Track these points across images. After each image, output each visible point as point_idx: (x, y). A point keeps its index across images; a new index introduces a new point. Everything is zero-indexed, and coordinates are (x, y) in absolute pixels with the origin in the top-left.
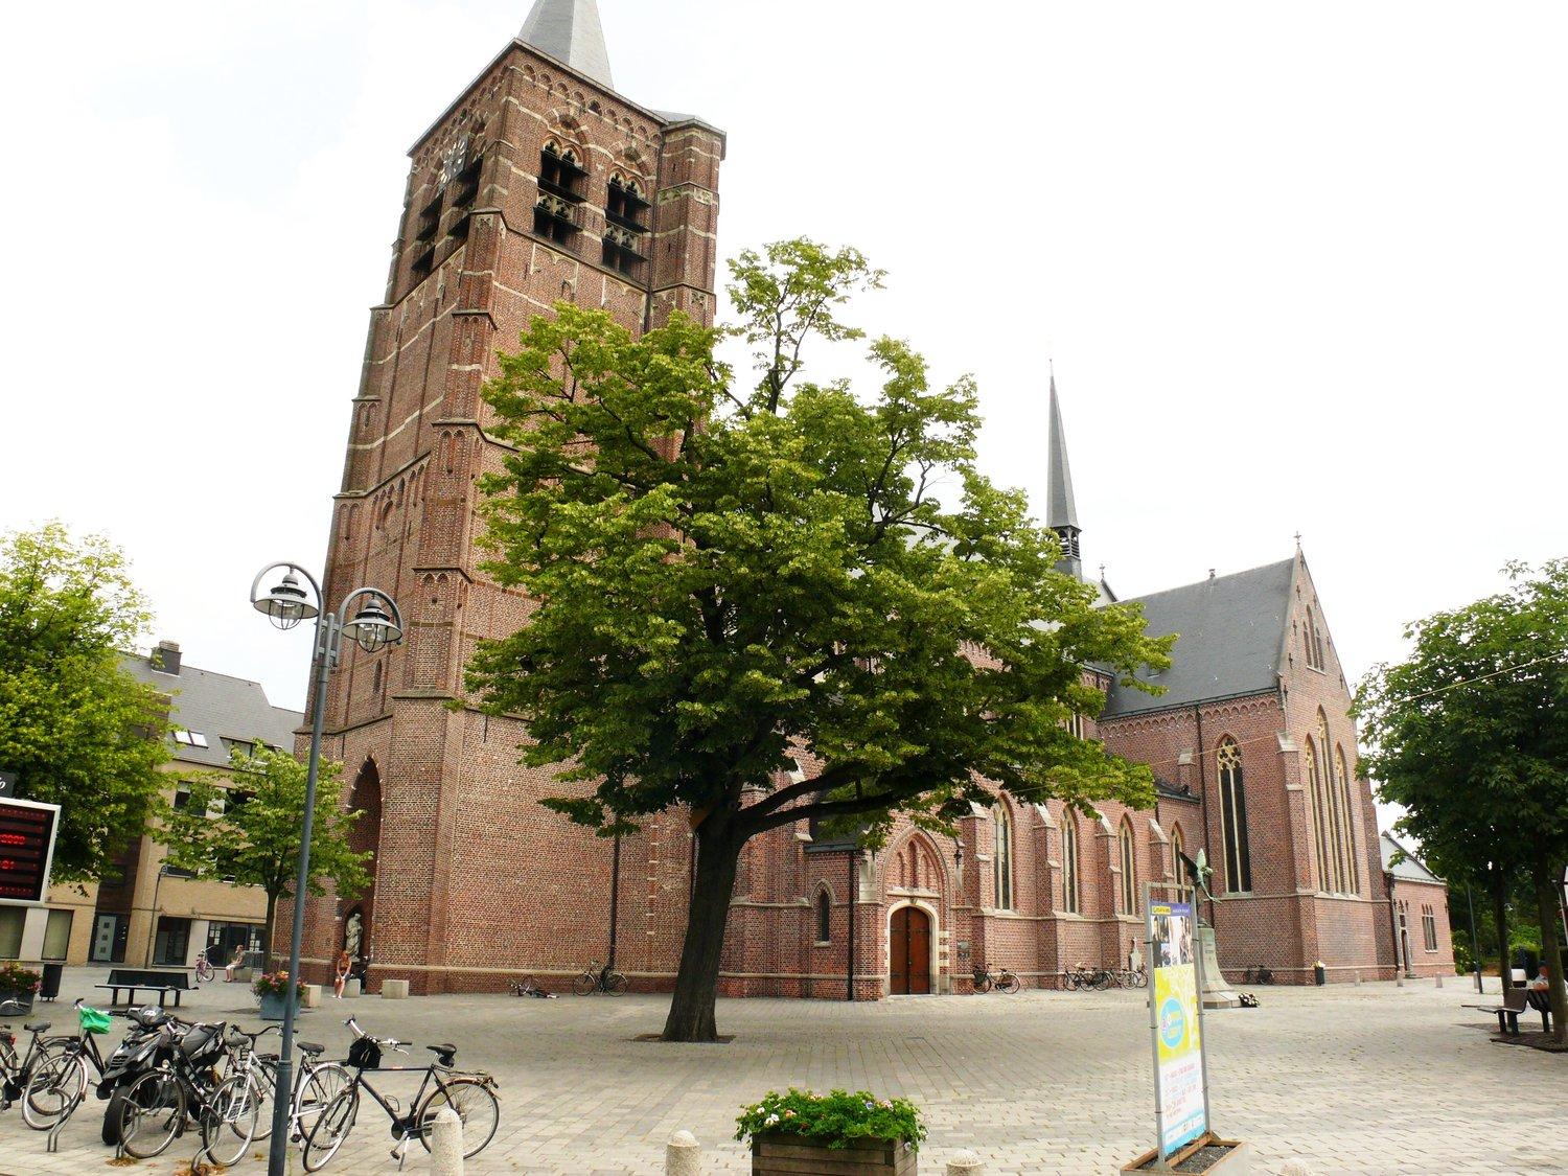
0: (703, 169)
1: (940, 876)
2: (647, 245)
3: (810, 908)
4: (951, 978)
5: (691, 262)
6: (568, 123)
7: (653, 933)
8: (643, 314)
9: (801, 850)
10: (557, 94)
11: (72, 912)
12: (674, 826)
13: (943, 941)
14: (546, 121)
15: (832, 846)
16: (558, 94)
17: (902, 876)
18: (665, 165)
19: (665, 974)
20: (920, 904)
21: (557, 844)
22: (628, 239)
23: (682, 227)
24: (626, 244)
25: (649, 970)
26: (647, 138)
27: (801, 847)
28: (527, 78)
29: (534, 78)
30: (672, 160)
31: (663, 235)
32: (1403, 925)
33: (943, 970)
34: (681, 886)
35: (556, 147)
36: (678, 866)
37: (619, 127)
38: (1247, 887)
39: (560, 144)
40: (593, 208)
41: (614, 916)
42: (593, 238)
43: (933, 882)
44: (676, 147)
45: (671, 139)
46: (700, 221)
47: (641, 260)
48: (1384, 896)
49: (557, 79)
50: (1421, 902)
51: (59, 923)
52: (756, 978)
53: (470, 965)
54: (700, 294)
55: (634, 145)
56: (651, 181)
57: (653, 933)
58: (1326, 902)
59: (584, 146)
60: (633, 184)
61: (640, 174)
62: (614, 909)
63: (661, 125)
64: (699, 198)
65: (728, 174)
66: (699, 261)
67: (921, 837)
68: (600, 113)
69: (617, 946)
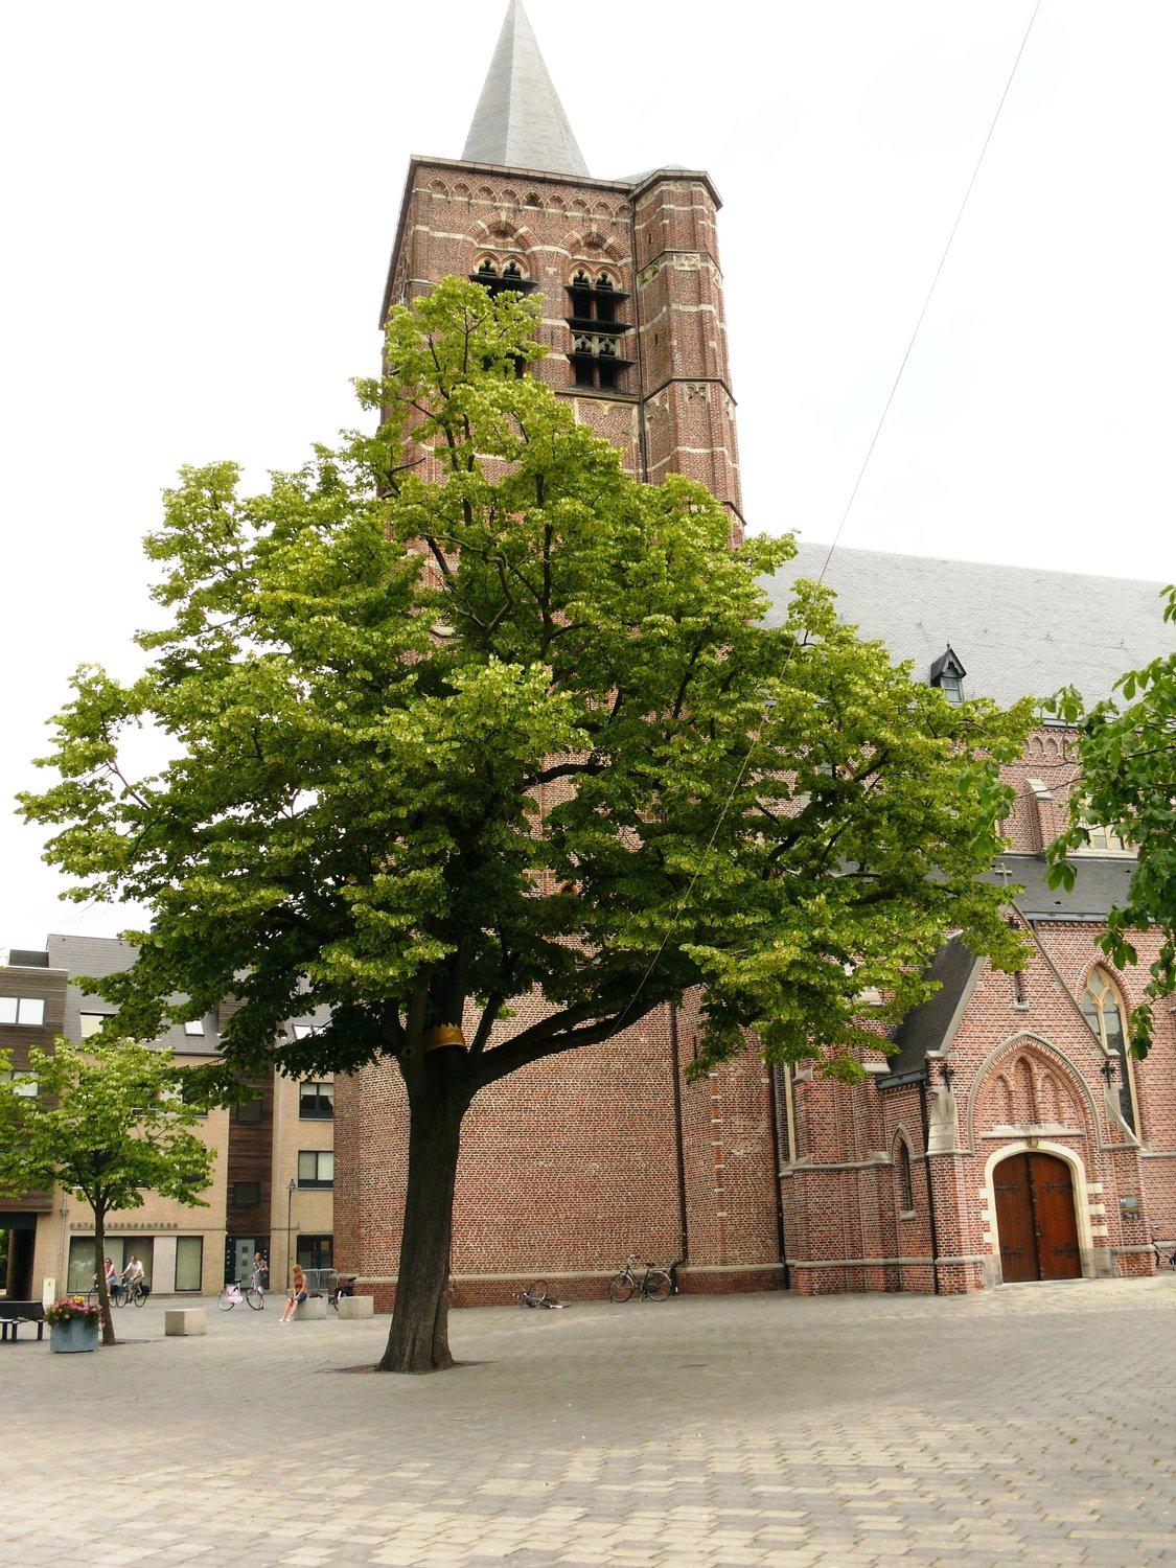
0: (681, 229)
1: (1078, 1102)
2: (631, 345)
3: (891, 1166)
4: (1114, 1253)
5: (681, 349)
6: (503, 231)
7: (724, 1214)
8: (636, 431)
9: (872, 1086)
10: (480, 202)
11: (201, 1238)
12: (740, 1071)
13: (1094, 1199)
14: (470, 239)
15: (900, 1077)
16: (484, 202)
17: (1010, 1109)
18: (641, 239)
19: (747, 1267)
20: (1045, 1146)
21: (592, 1111)
22: (607, 346)
23: (664, 309)
24: (607, 351)
25: (724, 1262)
26: (611, 214)
27: (872, 1082)
28: (439, 196)
29: (446, 193)
30: (647, 230)
31: (648, 326)
33: (1099, 1241)
34: (758, 1149)
35: (493, 264)
36: (751, 1123)
37: (569, 214)
39: (496, 259)
40: (548, 322)
41: (682, 1196)
43: (1068, 1113)
44: (649, 212)
45: (644, 204)
46: (688, 293)
47: (625, 365)
49: (569, 196)
51: (190, 1249)
52: (834, 1268)
53: (487, 1271)
54: (698, 385)
55: (594, 228)
56: (626, 265)
57: (724, 1214)
59: (528, 252)
60: (604, 276)
61: (609, 261)
62: (682, 1185)
63: (627, 192)
64: (682, 265)
65: (729, 229)
66: (692, 344)
67: (1035, 1050)
68: (541, 205)
69: (690, 1235)
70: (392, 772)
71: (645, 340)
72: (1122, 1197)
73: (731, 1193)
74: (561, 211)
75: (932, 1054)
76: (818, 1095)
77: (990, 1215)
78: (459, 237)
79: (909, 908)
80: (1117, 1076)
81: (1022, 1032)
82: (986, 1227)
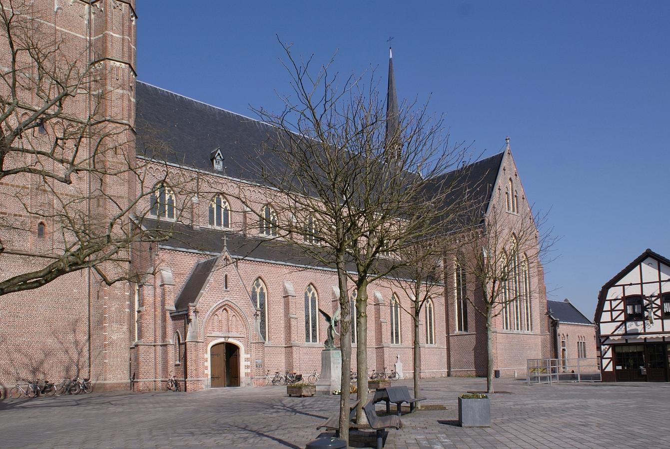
8: (87, 17)
32: (564, 345)
33: (247, 374)
48: (547, 332)
50: (577, 334)
58: (508, 335)
72: (256, 359)
73: (110, 353)
75: (190, 304)
76: (147, 317)
77: (208, 364)
80: (259, 317)
81: (226, 299)
82: (206, 368)
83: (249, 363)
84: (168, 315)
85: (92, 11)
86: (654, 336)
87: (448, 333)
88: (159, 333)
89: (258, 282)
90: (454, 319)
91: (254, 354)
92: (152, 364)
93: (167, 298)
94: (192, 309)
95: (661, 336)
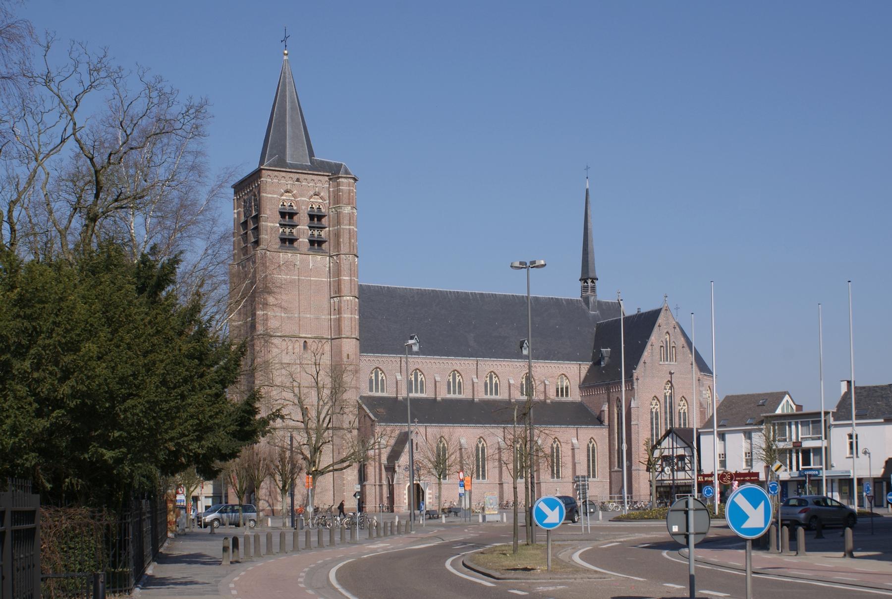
8: (328, 266)
13: (430, 494)
33: (430, 503)
38: (558, 477)
40: (303, 227)
42: (304, 240)
46: (346, 221)
70: (29, 217)
71: (331, 233)
74: (307, 184)
78: (275, 196)
79: (73, 396)
83: (431, 496)
84: (383, 467)
85: (331, 261)
86: (682, 481)
87: (610, 468)
88: (377, 478)
89: (441, 439)
90: (614, 456)
91: (434, 491)
92: (374, 496)
93: (382, 456)
94: (397, 465)
95: (684, 481)
